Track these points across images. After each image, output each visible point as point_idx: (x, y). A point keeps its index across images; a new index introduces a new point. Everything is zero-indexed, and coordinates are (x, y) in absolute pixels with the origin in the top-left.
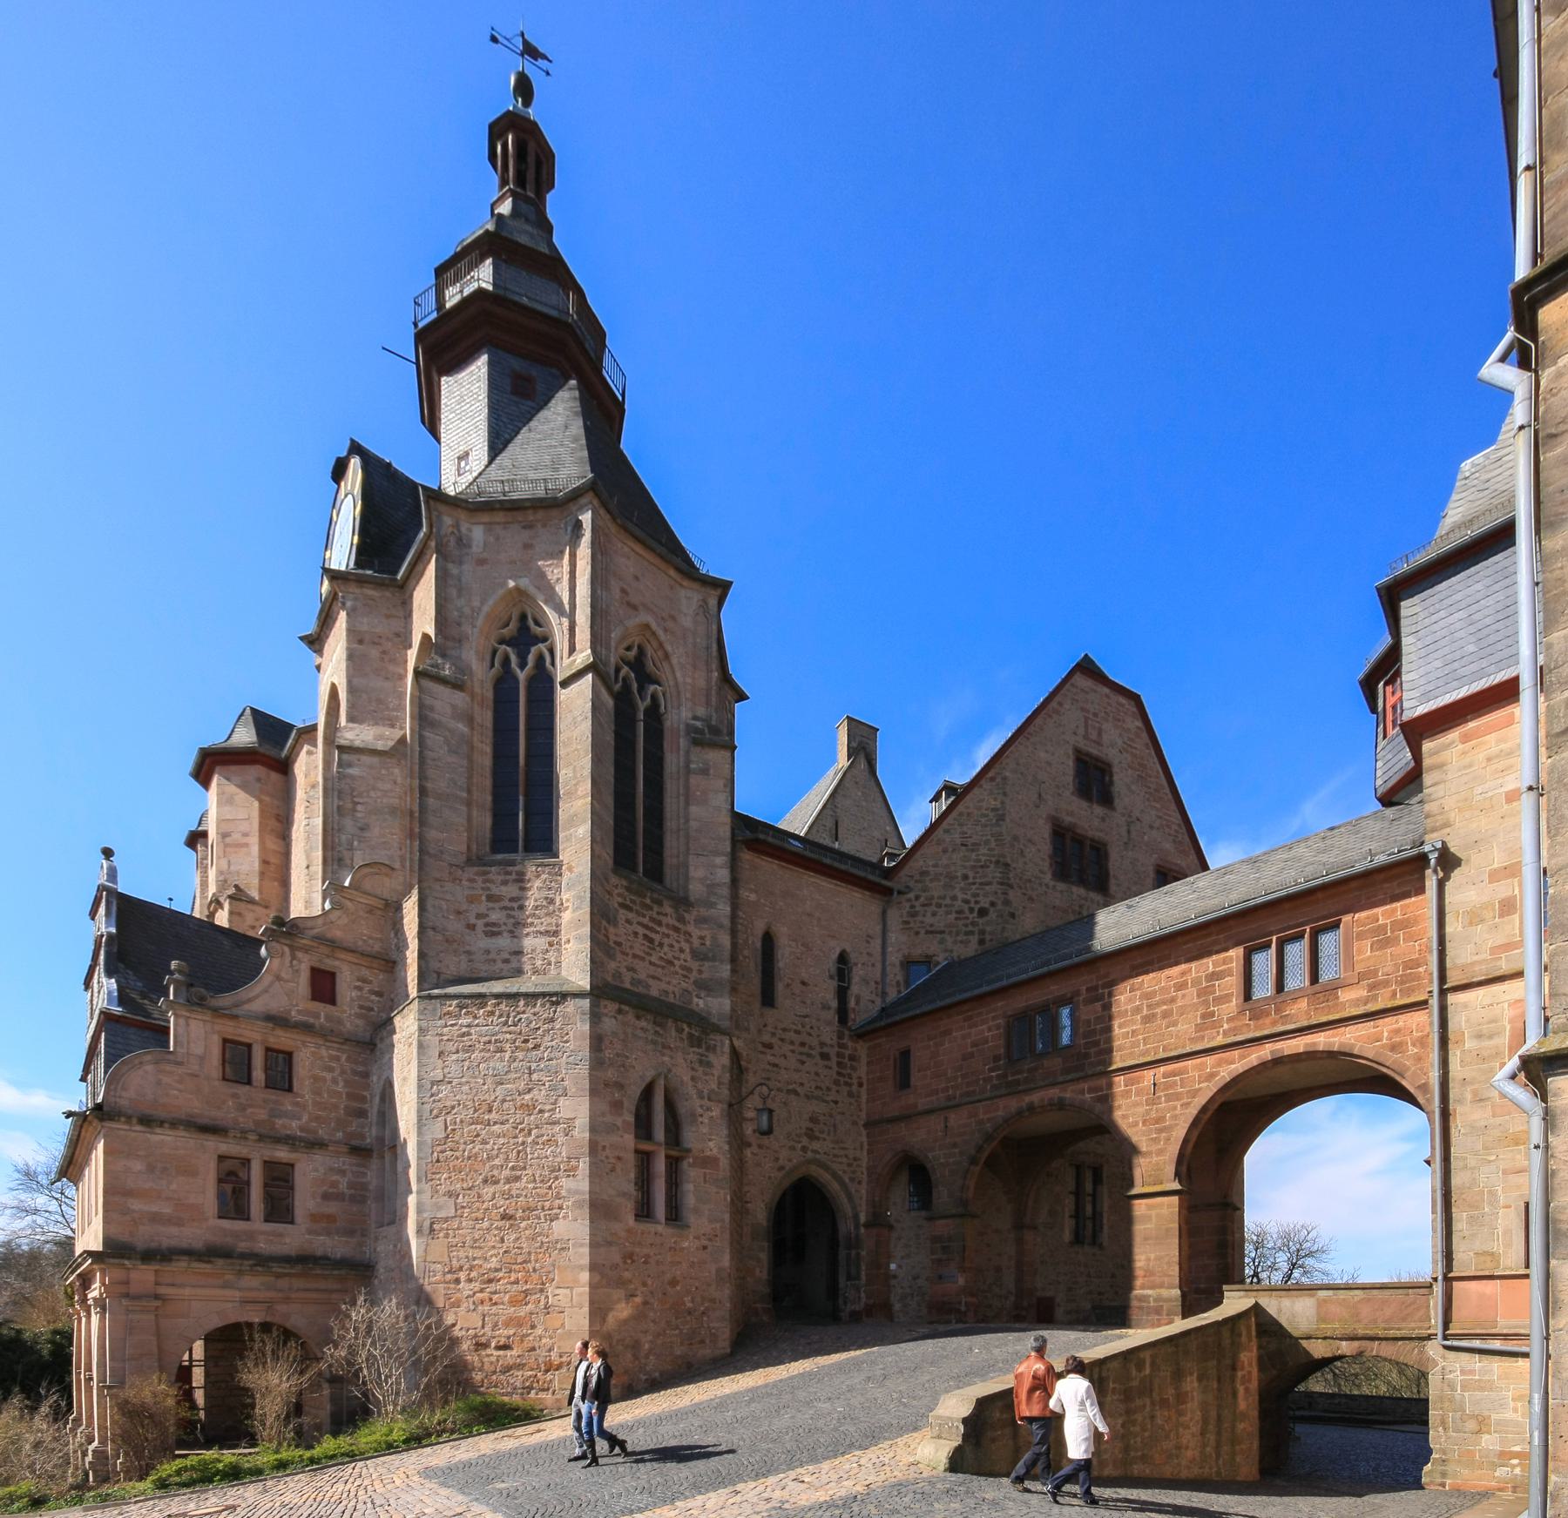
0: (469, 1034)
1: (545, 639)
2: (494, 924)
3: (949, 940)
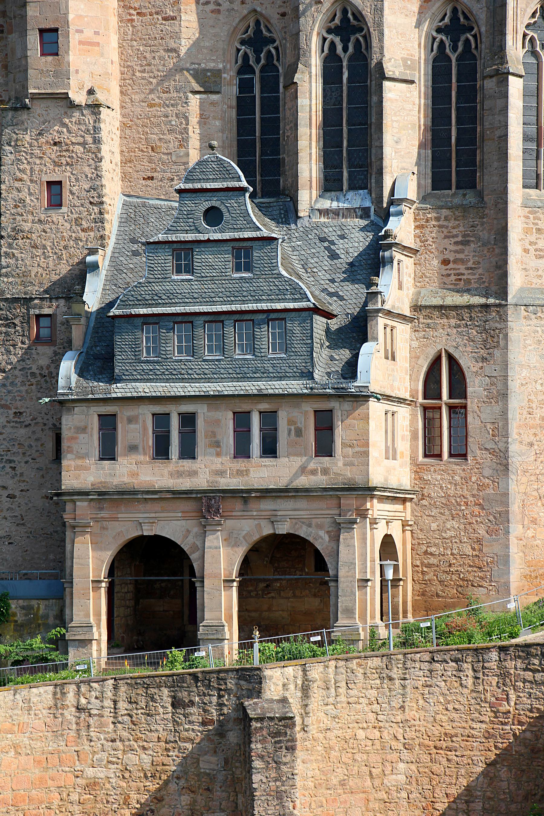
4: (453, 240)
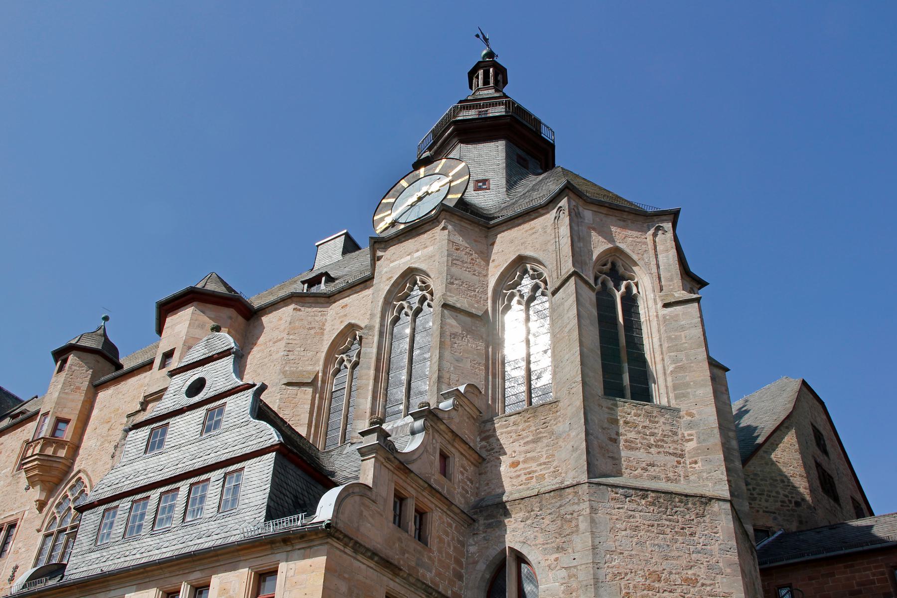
0: (634, 517)
3: (780, 518)
4: (522, 442)
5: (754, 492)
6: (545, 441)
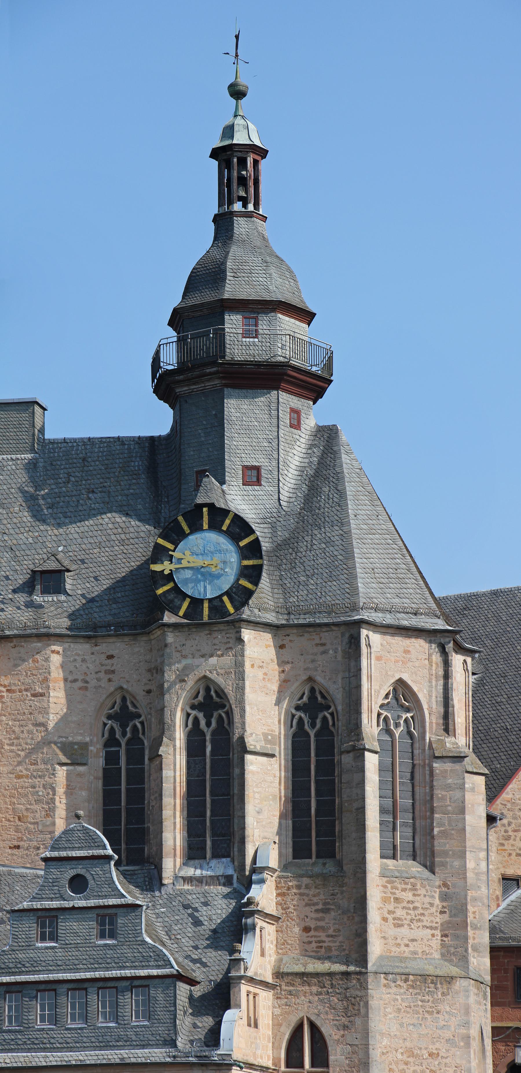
1: (223, 706)
2: (399, 919)
5: (509, 829)
6: (333, 913)
